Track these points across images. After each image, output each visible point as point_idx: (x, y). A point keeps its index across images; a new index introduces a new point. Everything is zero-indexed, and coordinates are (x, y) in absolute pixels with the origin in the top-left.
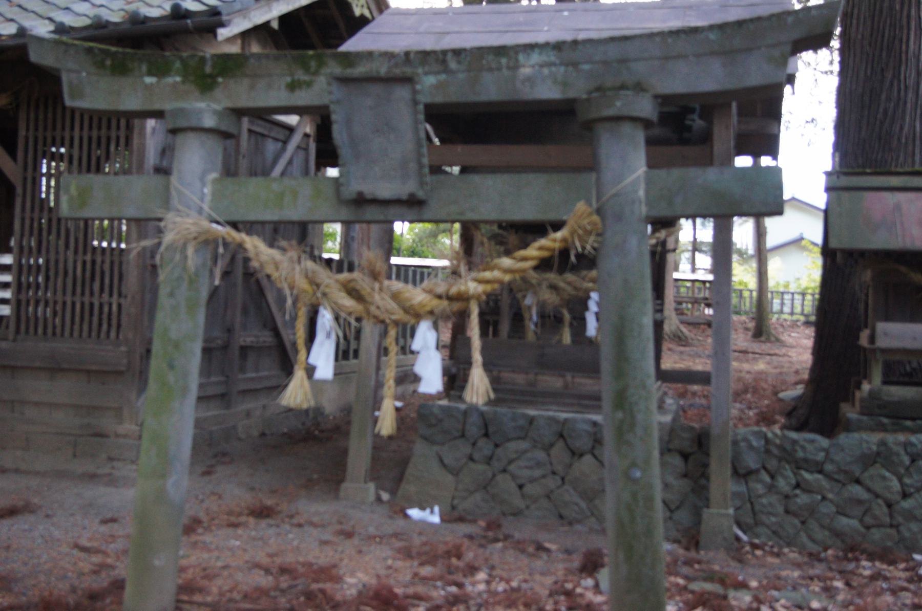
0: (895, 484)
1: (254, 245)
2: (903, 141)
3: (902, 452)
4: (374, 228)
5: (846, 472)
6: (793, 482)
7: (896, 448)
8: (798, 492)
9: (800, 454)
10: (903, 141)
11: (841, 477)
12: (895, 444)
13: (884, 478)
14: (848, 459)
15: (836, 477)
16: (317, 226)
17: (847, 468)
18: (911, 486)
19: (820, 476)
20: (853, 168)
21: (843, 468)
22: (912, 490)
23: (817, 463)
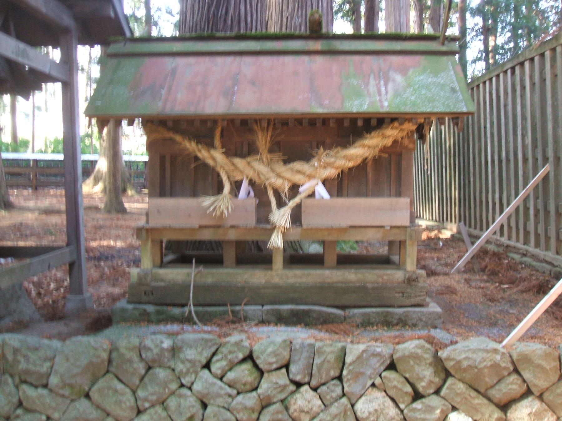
0: (128, 399)
1: (325, 356)
2: (229, 22)
3: (136, 359)
4: (382, 27)
5: (72, 386)
6: (15, 400)
7: (129, 354)
8: (19, 411)
9: (23, 365)
10: (229, 22)
11: (67, 392)
12: (127, 349)
13: (116, 391)
14: (75, 371)
15: (61, 392)
16: (188, 35)
17: (73, 381)
18: (146, 400)
19: (44, 392)
20: (310, 18)
21: (67, 381)
22: (147, 405)
23: (40, 375)
